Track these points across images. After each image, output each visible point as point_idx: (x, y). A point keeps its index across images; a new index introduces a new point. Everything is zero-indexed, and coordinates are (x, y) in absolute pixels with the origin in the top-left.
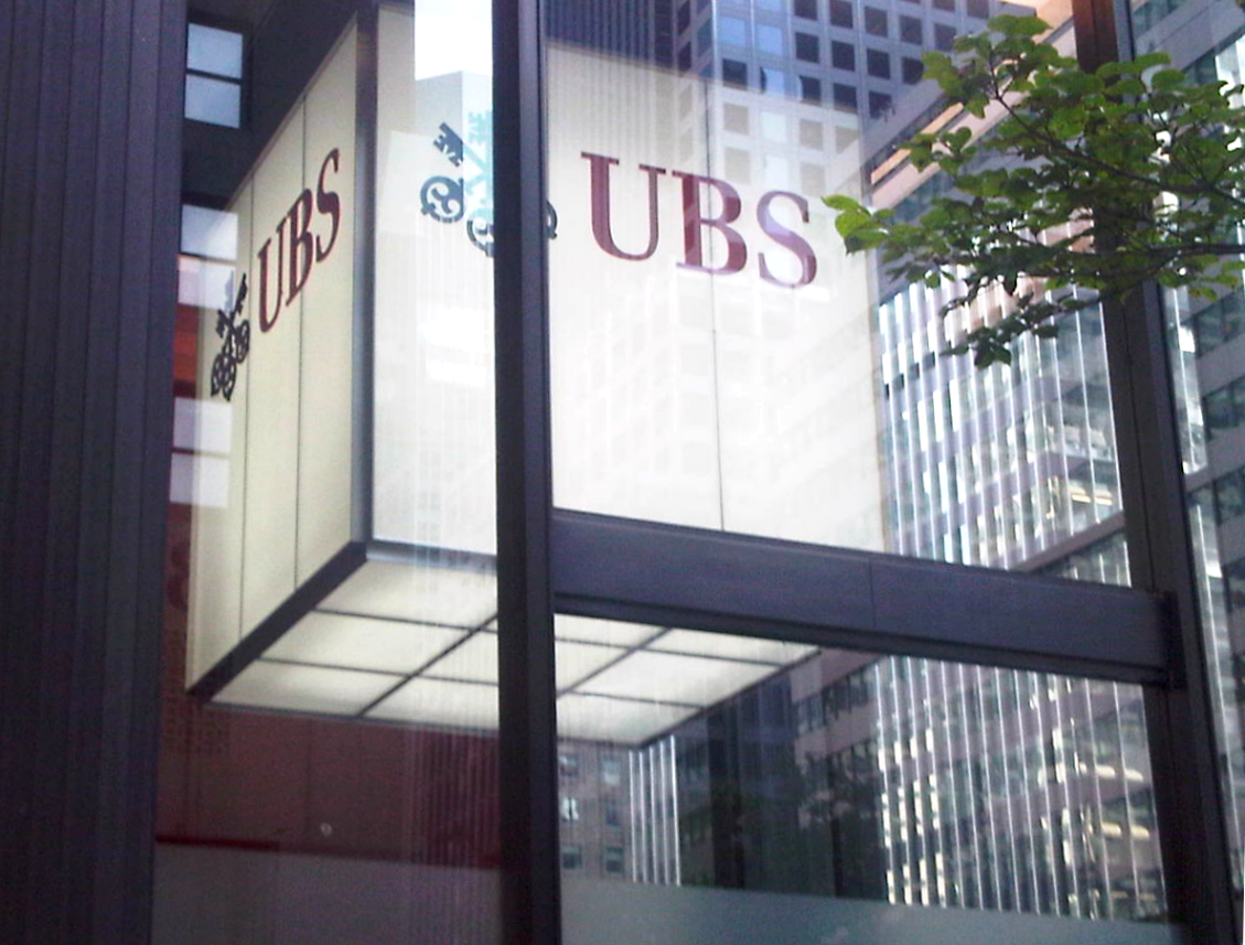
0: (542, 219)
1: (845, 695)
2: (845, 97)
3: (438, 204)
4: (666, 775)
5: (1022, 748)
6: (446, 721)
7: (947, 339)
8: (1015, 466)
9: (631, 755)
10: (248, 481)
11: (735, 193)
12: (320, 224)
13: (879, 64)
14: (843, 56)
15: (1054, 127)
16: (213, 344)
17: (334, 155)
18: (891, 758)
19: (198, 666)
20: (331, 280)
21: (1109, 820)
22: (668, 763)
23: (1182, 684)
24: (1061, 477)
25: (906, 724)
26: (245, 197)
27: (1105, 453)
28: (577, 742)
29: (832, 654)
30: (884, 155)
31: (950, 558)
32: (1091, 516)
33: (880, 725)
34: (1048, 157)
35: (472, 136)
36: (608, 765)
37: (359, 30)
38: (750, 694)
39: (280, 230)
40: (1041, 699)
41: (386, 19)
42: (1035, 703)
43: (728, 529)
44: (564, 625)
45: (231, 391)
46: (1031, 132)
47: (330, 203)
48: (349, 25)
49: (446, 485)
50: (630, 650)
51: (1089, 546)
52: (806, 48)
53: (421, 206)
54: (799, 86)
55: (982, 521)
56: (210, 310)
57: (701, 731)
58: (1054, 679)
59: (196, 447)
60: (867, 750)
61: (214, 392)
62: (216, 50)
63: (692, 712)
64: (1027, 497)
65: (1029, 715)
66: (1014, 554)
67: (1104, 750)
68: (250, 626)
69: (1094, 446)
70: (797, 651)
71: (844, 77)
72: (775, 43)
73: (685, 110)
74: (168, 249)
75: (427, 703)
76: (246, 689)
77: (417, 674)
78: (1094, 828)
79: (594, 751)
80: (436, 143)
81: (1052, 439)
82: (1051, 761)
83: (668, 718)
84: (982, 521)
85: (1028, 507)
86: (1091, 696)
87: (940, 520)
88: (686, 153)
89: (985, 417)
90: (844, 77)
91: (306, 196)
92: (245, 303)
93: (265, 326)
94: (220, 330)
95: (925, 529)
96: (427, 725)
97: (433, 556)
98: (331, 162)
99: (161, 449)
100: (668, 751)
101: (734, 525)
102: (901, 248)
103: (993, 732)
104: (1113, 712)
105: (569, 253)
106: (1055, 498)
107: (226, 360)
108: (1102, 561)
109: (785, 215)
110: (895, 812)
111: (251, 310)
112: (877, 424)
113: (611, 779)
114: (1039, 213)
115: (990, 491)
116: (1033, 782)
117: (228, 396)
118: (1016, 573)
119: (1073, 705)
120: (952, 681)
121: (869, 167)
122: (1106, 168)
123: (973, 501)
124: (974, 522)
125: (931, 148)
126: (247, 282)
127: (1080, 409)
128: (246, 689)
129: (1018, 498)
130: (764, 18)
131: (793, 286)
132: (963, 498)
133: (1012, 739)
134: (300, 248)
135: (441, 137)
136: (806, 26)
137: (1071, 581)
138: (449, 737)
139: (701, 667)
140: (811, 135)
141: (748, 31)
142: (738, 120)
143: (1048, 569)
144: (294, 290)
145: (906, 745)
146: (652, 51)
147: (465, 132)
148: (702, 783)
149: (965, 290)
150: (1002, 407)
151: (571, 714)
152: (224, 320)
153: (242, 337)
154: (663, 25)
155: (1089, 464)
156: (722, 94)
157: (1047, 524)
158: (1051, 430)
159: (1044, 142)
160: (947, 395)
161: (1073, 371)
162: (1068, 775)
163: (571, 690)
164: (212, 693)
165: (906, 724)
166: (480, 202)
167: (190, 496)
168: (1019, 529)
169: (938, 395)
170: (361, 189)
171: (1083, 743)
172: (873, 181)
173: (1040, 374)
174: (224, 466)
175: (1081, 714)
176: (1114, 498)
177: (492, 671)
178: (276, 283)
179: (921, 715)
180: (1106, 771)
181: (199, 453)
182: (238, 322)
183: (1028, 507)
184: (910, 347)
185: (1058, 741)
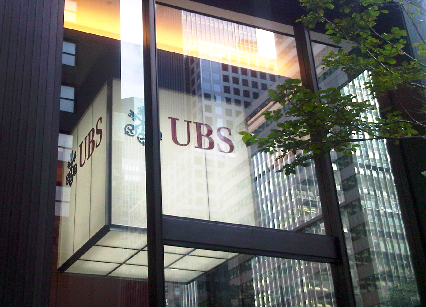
0: (159, 135)
1: (244, 267)
2: (238, 102)
3: (129, 131)
4: (194, 291)
5: (294, 282)
6: (130, 277)
7: (268, 167)
8: (289, 202)
9: (183, 285)
10: (76, 210)
11: (211, 129)
12: (97, 137)
13: (246, 94)
14: (237, 92)
15: (304, 108)
16: (66, 171)
17: (101, 119)
18: (257, 286)
19: (61, 262)
20: (100, 153)
21: (320, 303)
22: (193, 288)
23: (342, 263)
24: (302, 205)
25: (261, 276)
26: (76, 131)
27: (314, 198)
28: (168, 282)
29: (242, 255)
30: (249, 118)
31: (271, 227)
32: (310, 217)
33: (253, 276)
34: (303, 116)
35: (138, 114)
36: (176, 289)
37: (107, 86)
38: (217, 268)
39: (86, 139)
40: (298, 268)
41: (115, 82)
42: (297, 269)
43: (212, 220)
44: (166, 248)
45: (71, 183)
46: (298, 110)
47: (99, 132)
48: (105, 84)
49: (133, 207)
50: (185, 255)
51: (314, 223)
52: (227, 90)
53: (124, 132)
54: (225, 99)
55: (280, 218)
56: (66, 162)
57: (204, 279)
58: (302, 262)
59: (61, 200)
60: (250, 284)
61: (67, 184)
62: (68, 92)
63: (202, 273)
64: (292, 211)
65: (295, 273)
66: (289, 227)
67: (318, 282)
68: (76, 250)
69: (310, 197)
70: (230, 255)
71: (237, 97)
72: (218, 88)
73: (194, 106)
74: (55, 146)
75: (126, 271)
76: (74, 269)
77: (124, 263)
78: (315, 305)
79: (172, 284)
80: (128, 115)
81: (299, 195)
82: (302, 286)
83: (195, 275)
84: (280, 218)
85: (293, 213)
86: (313, 267)
87: (269, 217)
88: (195, 117)
89: (280, 188)
90: (237, 97)
91: (93, 130)
92: (76, 159)
93: (81, 166)
94: (68, 167)
95: (264, 220)
96: (124, 278)
97: (126, 229)
98: (100, 120)
99: (53, 201)
100: (193, 285)
101: (217, 217)
102: (257, 143)
103: (285, 278)
104: (319, 272)
105: (166, 144)
106: (300, 211)
107: (70, 175)
108: (314, 229)
109: (224, 133)
110: (258, 301)
111: (77, 161)
112: (252, 189)
113: (177, 293)
114: (301, 132)
115: (282, 209)
116: (297, 292)
117: (70, 185)
118: (290, 232)
119: (308, 270)
120: (274, 264)
121: (247, 120)
122: (320, 119)
123: (277, 212)
124: (278, 218)
125: (270, 115)
126: (76, 153)
127: (306, 186)
128: (74, 269)
129: (290, 211)
130: (215, 82)
131: (228, 152)
132: (274, 211)
133: (291, 279)
134: (91, 144)
135: (130, 113)
136: (226, 84)
137: (306, 233)
138: (131, 281)
139: (203, 260)
140: (228, 112)
141: (211, 86)
142: (209, 109)
143: (301, 230)
144: (89, 156)
145: (261, 282)
146: (185, 90)
147: (136, 112)
148: (205, 294)
149: (282, 153)
150: (284, 186)
151: (168, 274)
152: (70, 164)
153: (75, 169)
154: (188, 84)
155: (309, 201)
156: (205, 102)
157: (298, 218)
158: (298, 192)
159: (302, 112)
160: (269, 182)
161: (304, 176)
162: (307, 290)
163: (167, 267)
164: (64, 270)
165: (261, 276)
166: (141, 131)
167: (60, 214)
168: (291, 220)
169: (266, 183)
170: (108, 128)
171: (311, 281)
172: (248, 124)
173: (294, 176)
174: (68, 204)
175: (310, 273)
176: (317, 211)
177: (146, 262)
178: (84, 154)
179: (265, 273)
180: (318, 289)
181: (62, 201)
182: (73, 164)
183: (293, 213)
184: (258, 170)
185: (304, 280)
